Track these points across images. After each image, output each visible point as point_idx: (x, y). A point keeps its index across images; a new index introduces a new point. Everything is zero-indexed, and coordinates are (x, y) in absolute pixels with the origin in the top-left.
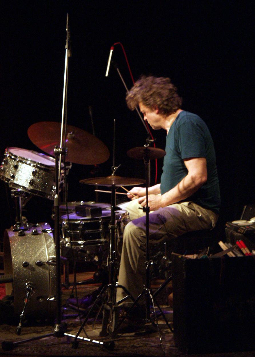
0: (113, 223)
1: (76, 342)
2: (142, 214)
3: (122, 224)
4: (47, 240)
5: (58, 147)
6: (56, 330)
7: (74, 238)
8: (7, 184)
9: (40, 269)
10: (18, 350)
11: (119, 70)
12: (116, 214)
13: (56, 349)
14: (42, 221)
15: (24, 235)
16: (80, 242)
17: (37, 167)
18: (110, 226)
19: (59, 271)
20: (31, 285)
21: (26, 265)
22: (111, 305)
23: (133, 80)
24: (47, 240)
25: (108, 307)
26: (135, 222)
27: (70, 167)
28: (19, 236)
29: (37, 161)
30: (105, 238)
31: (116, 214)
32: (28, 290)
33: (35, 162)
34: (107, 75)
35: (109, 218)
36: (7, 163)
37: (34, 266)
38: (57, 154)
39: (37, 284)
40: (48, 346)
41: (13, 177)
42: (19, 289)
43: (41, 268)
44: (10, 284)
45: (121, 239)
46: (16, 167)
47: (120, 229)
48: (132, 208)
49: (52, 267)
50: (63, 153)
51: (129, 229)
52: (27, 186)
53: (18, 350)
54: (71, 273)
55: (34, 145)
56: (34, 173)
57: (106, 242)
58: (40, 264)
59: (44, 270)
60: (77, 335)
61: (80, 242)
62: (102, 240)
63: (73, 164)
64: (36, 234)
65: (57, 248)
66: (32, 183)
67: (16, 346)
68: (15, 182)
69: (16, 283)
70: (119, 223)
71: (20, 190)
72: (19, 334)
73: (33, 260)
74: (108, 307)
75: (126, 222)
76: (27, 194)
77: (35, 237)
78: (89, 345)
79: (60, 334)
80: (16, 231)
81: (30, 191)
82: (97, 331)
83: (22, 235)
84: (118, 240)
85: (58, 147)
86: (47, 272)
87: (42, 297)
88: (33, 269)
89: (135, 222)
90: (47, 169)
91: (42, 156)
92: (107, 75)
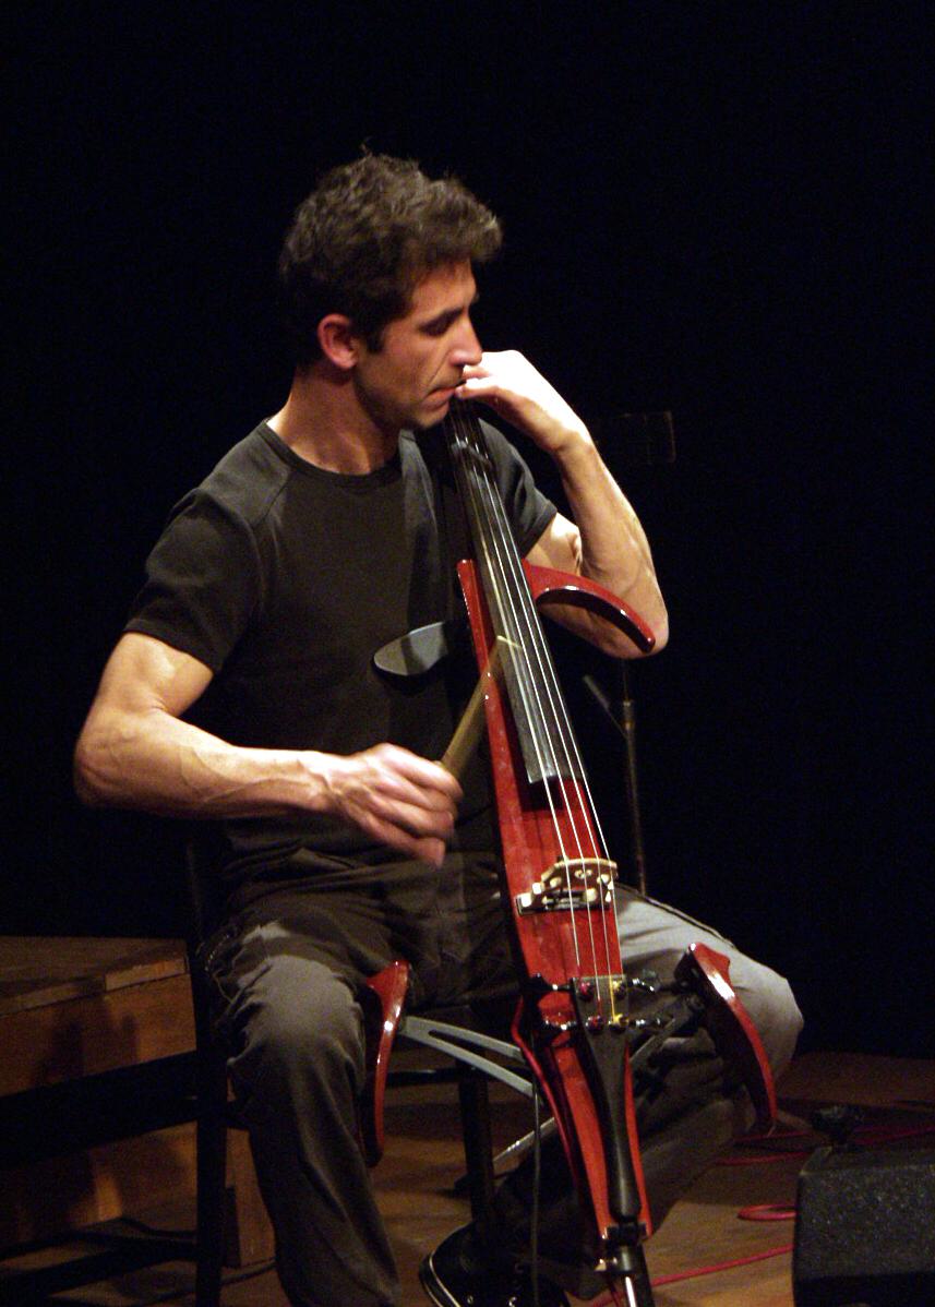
34: (587, 680)
92: (587, 680)
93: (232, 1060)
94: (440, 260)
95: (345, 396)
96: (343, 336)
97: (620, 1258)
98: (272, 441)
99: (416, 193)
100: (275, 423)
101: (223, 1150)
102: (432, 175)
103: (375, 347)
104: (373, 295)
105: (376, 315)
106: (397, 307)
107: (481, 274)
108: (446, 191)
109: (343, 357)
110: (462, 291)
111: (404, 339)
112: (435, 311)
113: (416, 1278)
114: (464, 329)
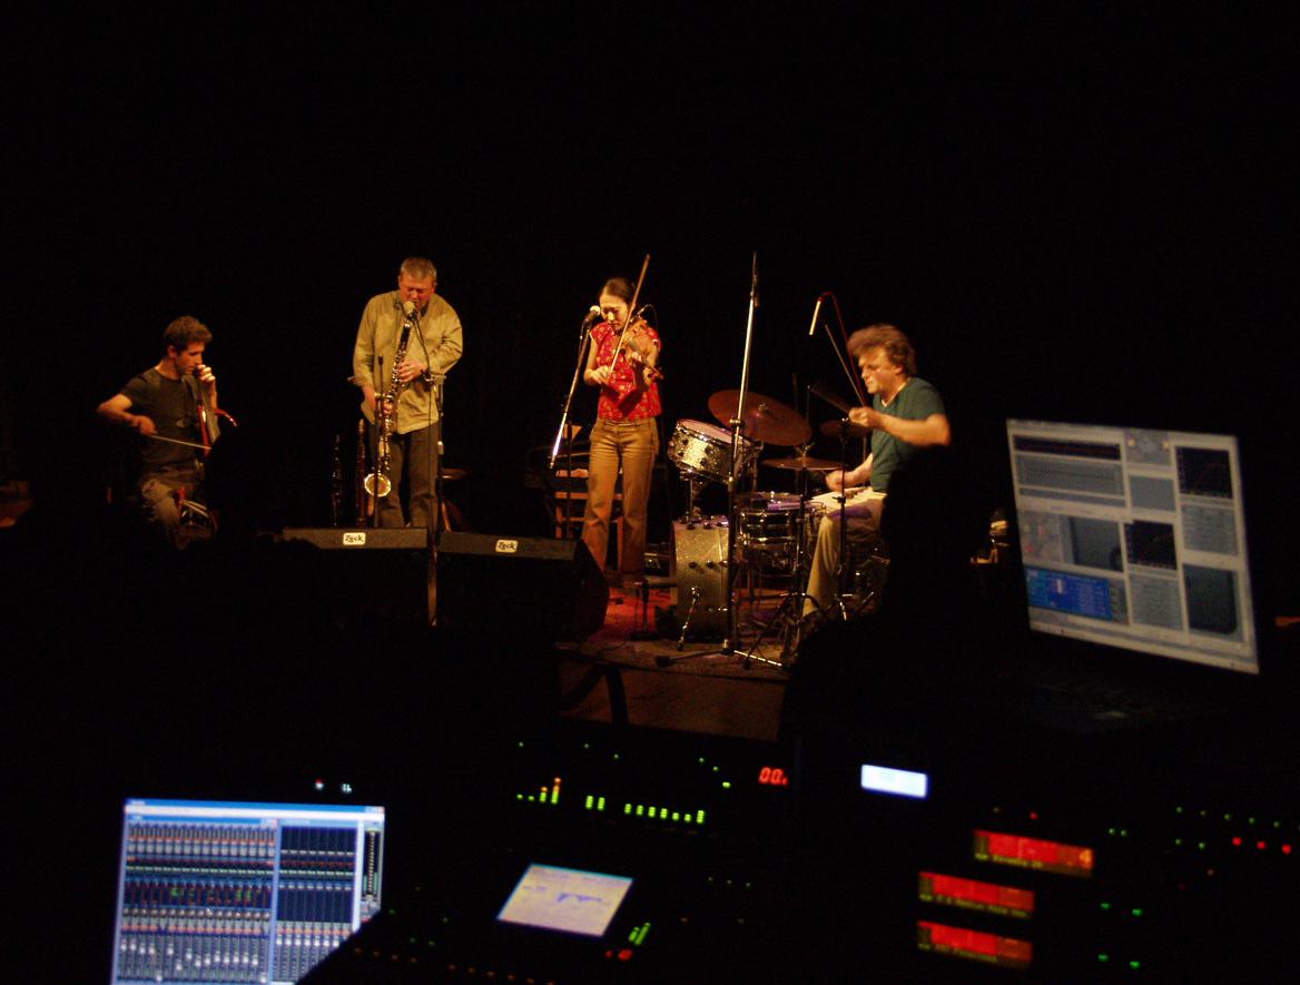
0: (802, 517)
1: (748, 663)
2: (839, 507)
3: (816, 519)
4: (721, 536)
5: (735, 418)
6: (725, 646)
7: (755, 534)
8: (679, 470)
9: (710, 571)
10: (675, 667)
11: (821, 306)
12: (807, 506)
13: (721, 668)
14: (718, 512)
15: (694, 528)
16: (761, 539)
17: (712, 443)
18: (798, 520)
19: (731, 576)
20: (698, 590)
21: (693, 565)
22: (795, 620)
23: (844, 333)
24: (721, 536)
25: (792, 623)
26: (831, 516)
27: (762, 448)
28: (427, 373)
29: (712, 436)
30: (793, 535)
31: (807, 506)
32: (695, 596)
33: (708, 437)
34: (811, 333)
35: (797, 510)
36: (677, 437)
37: (703, 566)
38: (735, 426)
39: (706, 591)
40: (714, 665)
41: (682, 454)
42: (685, 596)
43: (712, 570)
44: (676, 589)
45: (815, 539)
46: (686, 442)
47: (812, 526)
48: (827, 502)
49: (725, 570)
50: (742, 425)
51: (825, 524)
52: (698, 466)
53: (675, 667)
54: (757, 586)
55: (715, 419)
56: (707, 450)
57: (793, 541)
58: (711, 565)
59: (716, 573)
60: (750, 653)
61: (761, 539)
62: (789, 538)
63: (765, 445)
64: (708, 527)
65: (732, 550)
66: (704, 463)
67: (674, 662)
68: (685, 462)
69: (682, 586)
70: (812, 518)
71: (690, 471)
72: (680, 649)
73: (702, 560)
74: (792, 623)
75: (820, 516)
76: (700, 479)
77: (708, 531)
78: (763, 668)
79: (729, 652)
80: (684, 522)
81: (701, 472)
82: (777, 653)
83: (691, 528)
84: (810, 539)
85: (735, 418)
86: (719, 575)
87: (712, 607)
88: (702, 571)
89: (831, 516)
90: (723, 446)
91: (725, 432)
92: (811, 333)
93: (685, 627)
94: (197, 340)
95: (171, 364)
96: (173, 351)
97: (760, 518)
98: (156, 372)
99: (196, 326)
100: (157, 368)
101: (973, 878)
102: (201, 322)
103: (179, 355)
104: (181, 344)
105: (181, 347)
106: (184, 348)
107: (207, 346)
108: (203, 328)
109: (172, 355)
110: (201, 348)
111: (185, 355)
112: (192, 351)
113: (693, 560)
114: (199, 357)
